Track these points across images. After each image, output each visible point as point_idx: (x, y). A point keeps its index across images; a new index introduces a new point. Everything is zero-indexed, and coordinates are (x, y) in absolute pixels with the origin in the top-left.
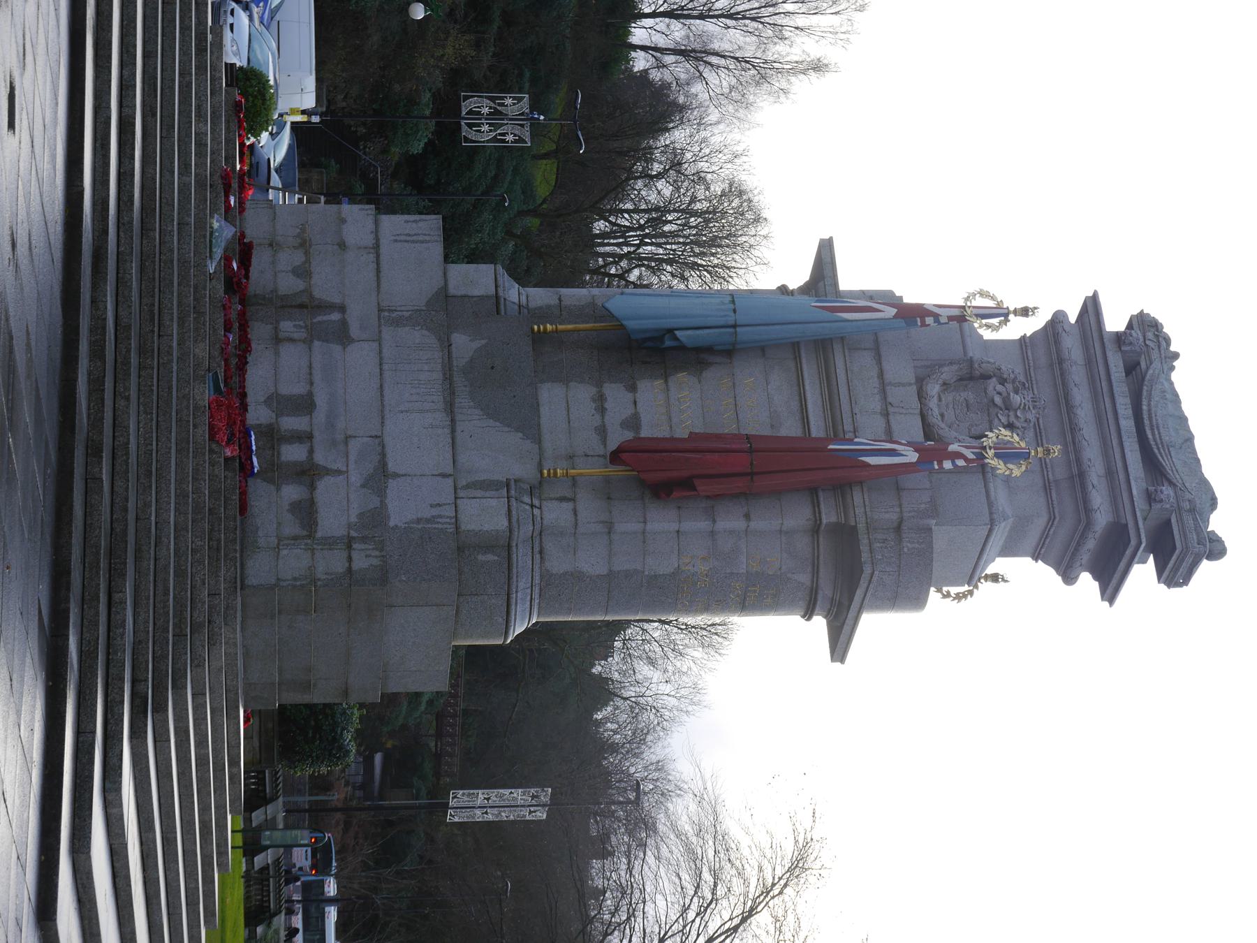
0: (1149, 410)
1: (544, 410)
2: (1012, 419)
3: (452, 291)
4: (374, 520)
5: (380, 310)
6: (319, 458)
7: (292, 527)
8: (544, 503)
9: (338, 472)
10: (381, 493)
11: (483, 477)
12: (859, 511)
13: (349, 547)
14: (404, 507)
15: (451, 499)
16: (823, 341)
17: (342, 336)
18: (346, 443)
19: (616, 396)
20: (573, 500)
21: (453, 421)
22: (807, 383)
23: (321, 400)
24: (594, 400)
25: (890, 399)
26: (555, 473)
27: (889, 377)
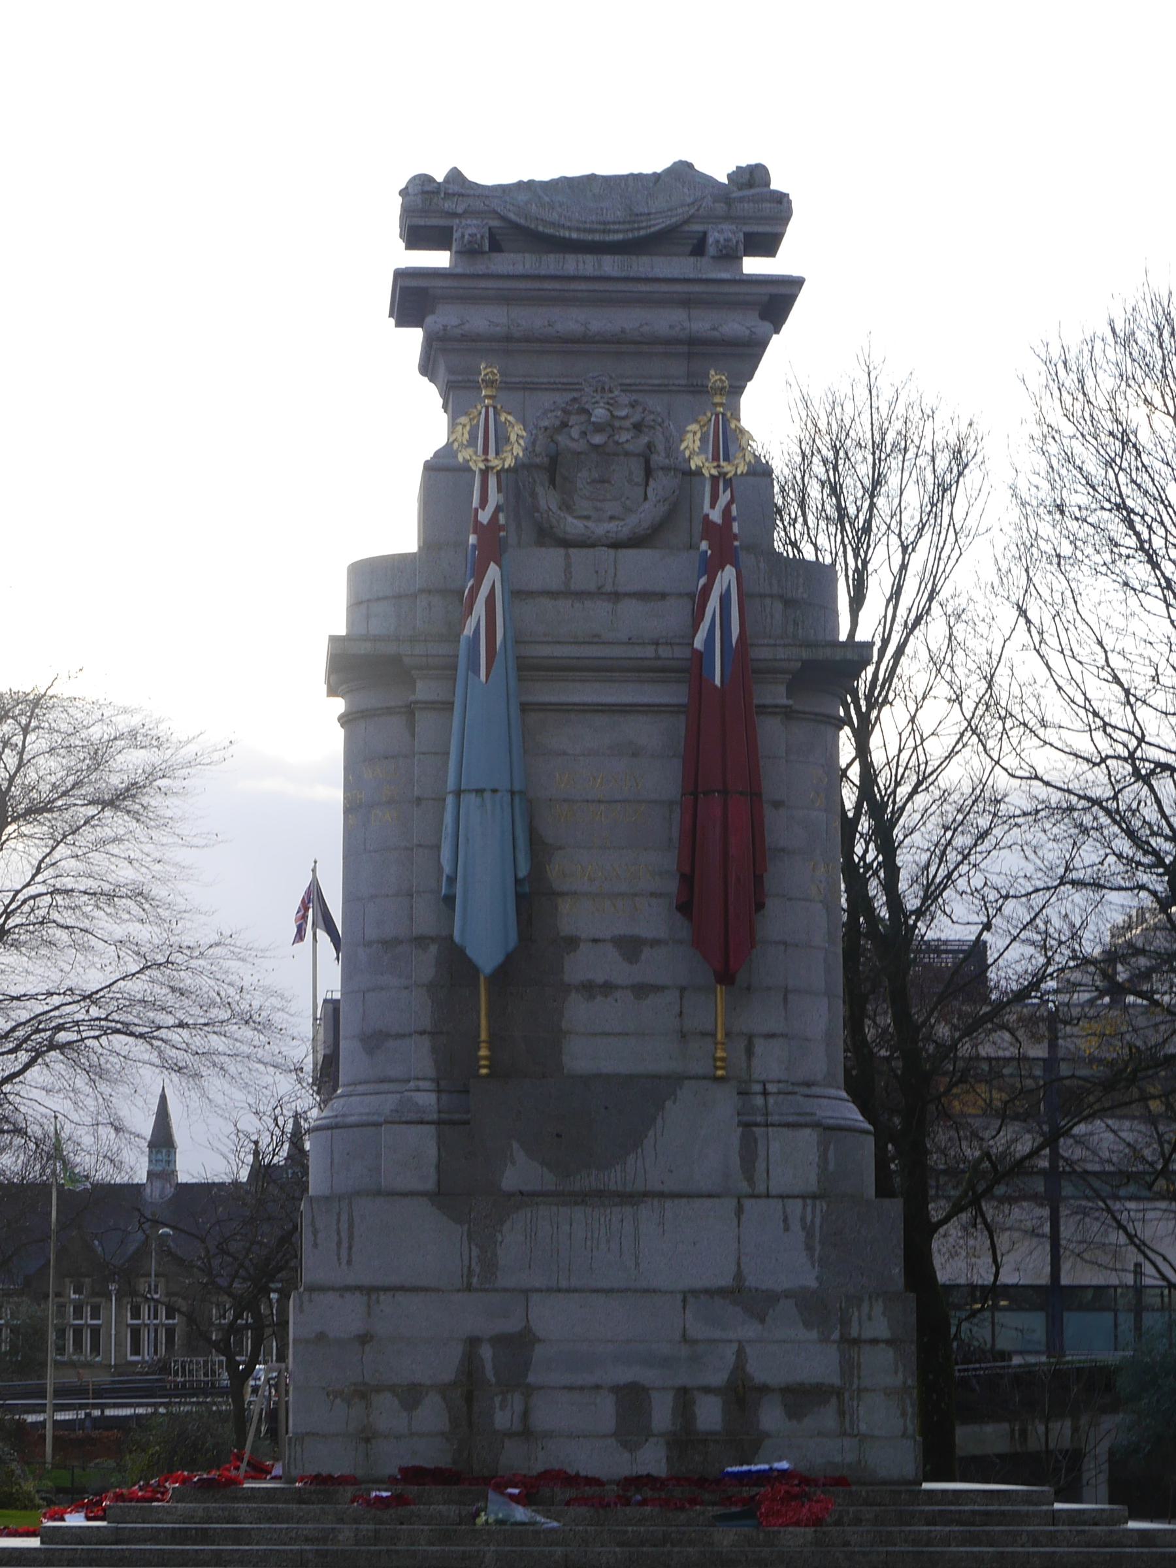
0: (578, 230)
1: (607, 1066)
2: (627, 424)
3: (430, 1185)
4: (813, 1308)
5: (469, 1288)
6: (718, 1378)
7: (827, 1417)
8: (755, 1076)
9: (740, 1354)
10: (772, 1297)
11: (736, 1160)
12: (781, 653)
13: (856, 1342)
14: (788, 1265)
15: (777, 1204)
16: (520, 668)
17: (519, 1345)
18: (695, 1342)
19: (582, 966)
20: (750, 1038)
21: (646, 1194)
22: (563, 699)
23: (624, 1375)
24: (592, 997)
25: (592, 587)
26: (723, 1059)
27: (555, 584)
